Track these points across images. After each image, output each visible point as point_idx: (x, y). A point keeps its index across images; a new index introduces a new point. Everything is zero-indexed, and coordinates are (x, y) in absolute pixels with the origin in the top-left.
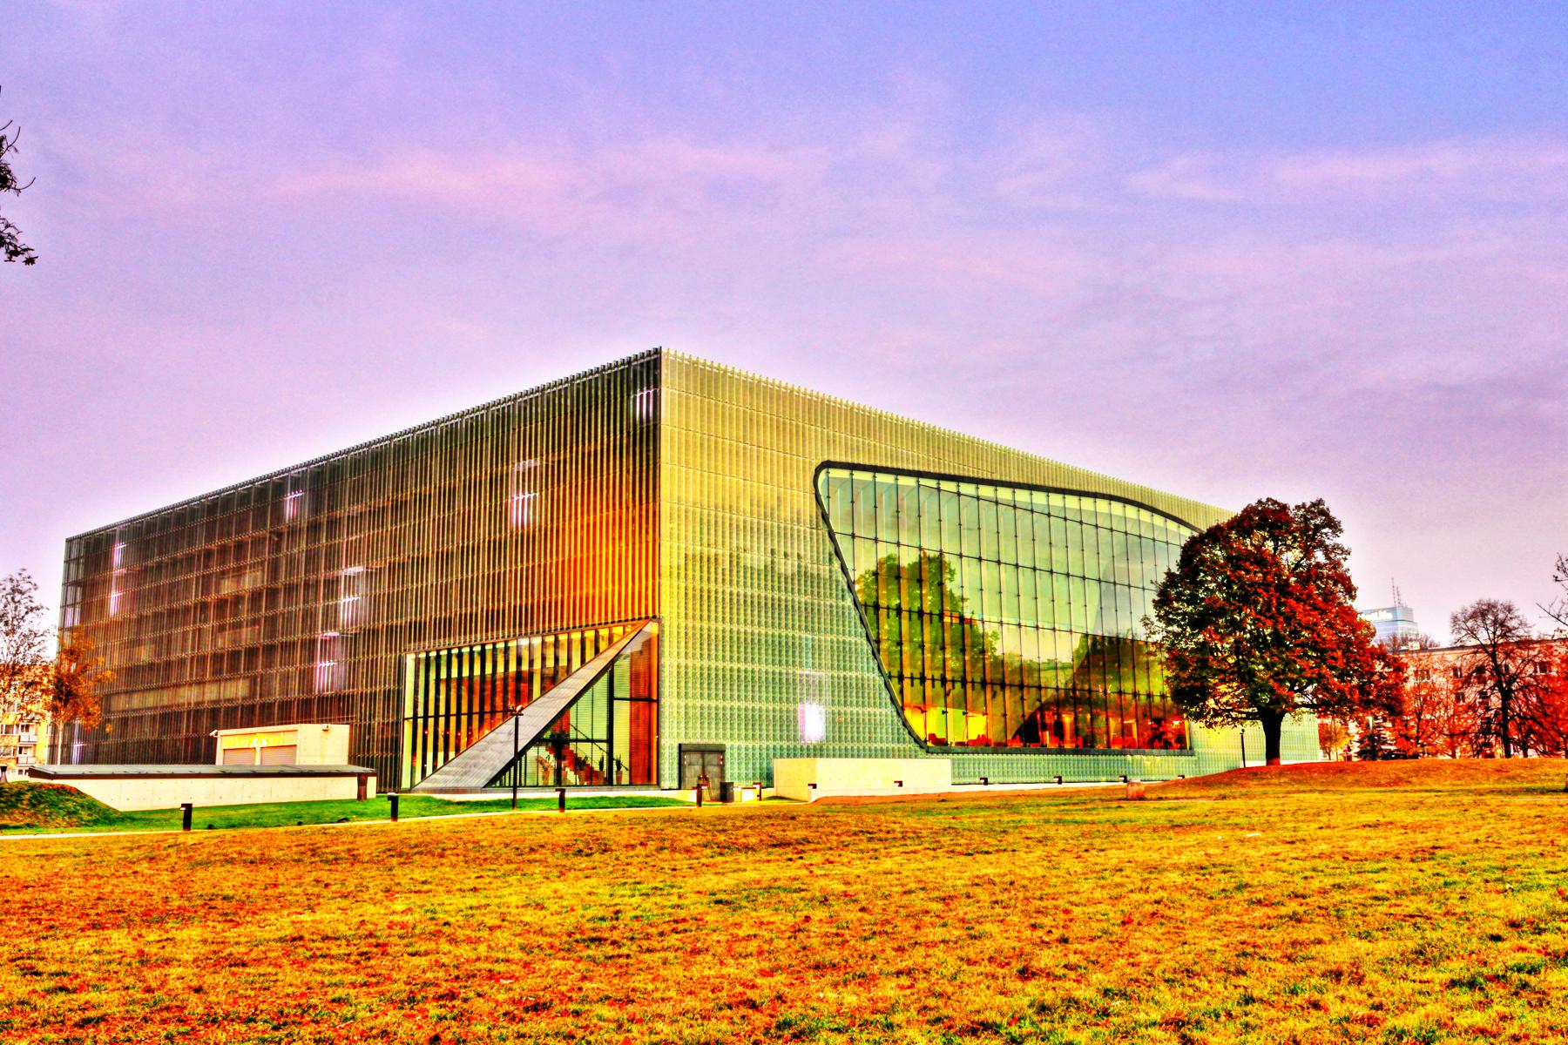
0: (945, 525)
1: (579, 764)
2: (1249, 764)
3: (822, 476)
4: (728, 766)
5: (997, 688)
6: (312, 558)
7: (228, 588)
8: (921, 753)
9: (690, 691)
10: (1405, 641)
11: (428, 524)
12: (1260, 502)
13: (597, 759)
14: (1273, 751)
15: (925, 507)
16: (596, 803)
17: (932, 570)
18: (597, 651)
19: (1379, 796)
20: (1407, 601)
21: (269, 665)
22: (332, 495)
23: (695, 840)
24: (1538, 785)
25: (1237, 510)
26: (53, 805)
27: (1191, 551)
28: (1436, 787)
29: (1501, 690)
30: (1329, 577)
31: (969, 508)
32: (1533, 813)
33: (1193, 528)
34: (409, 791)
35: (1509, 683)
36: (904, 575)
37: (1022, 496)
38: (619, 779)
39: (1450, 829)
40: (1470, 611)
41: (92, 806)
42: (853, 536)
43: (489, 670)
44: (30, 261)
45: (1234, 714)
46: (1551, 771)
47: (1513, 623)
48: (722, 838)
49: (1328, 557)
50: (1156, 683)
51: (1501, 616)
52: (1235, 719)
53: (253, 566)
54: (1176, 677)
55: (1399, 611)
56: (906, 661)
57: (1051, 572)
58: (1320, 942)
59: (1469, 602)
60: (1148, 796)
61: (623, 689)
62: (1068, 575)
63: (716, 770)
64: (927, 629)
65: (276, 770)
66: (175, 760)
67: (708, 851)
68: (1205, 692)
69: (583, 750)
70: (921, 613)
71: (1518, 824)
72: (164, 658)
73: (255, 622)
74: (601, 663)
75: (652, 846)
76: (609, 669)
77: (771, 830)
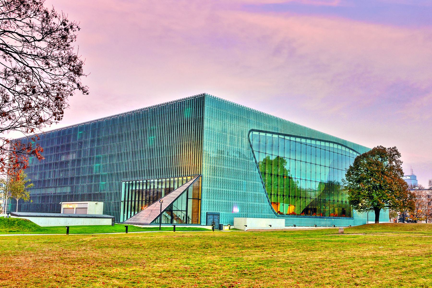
0: (286, 149)
1: (178, 219)
2: (369, 222)
3: (251, 134)
4: (220, 219)
5: (299, 198)
6: (92, 150)
7: (63, 158)
8: (276, 217)
10: (415, 187)
11: (130, 142)
12: (378, 147)
13: (183, 215)
14: (377, 219)
16: (183, 229)
17: (280, 161)
18: (182, 184)
19: (408, 235)
20: (415, 173)
23: (234, 245)
26: (24, 225)
27: (357, 160)
28: (423, 232)
31: (298, 146)
33: (357, 153)
34: (122, 223)
36: (273, 164)
37: (309, 141)
38: (189, 222)
41: (35, 225)
42: (259, 152)
43: (148, 188)
44: (88, 94)
45: (366, 208)
48: (241, 244)
49: (396, 164)
50: (345, 197)
53: (73, 153)
54: (351, 197)
55: (413, 177)
57: (316, 164)
58: (415, 279)
60: (344, 232)
61: (190, 196)
62: (321, 165)
63: (217, 220)
64: (279, 180)
67: (238, 248)
68: (358, 202)
69: (179, 213)
70: (278, 176)
73: (73, 169)
74: (184, 188)
76: (187, 190)
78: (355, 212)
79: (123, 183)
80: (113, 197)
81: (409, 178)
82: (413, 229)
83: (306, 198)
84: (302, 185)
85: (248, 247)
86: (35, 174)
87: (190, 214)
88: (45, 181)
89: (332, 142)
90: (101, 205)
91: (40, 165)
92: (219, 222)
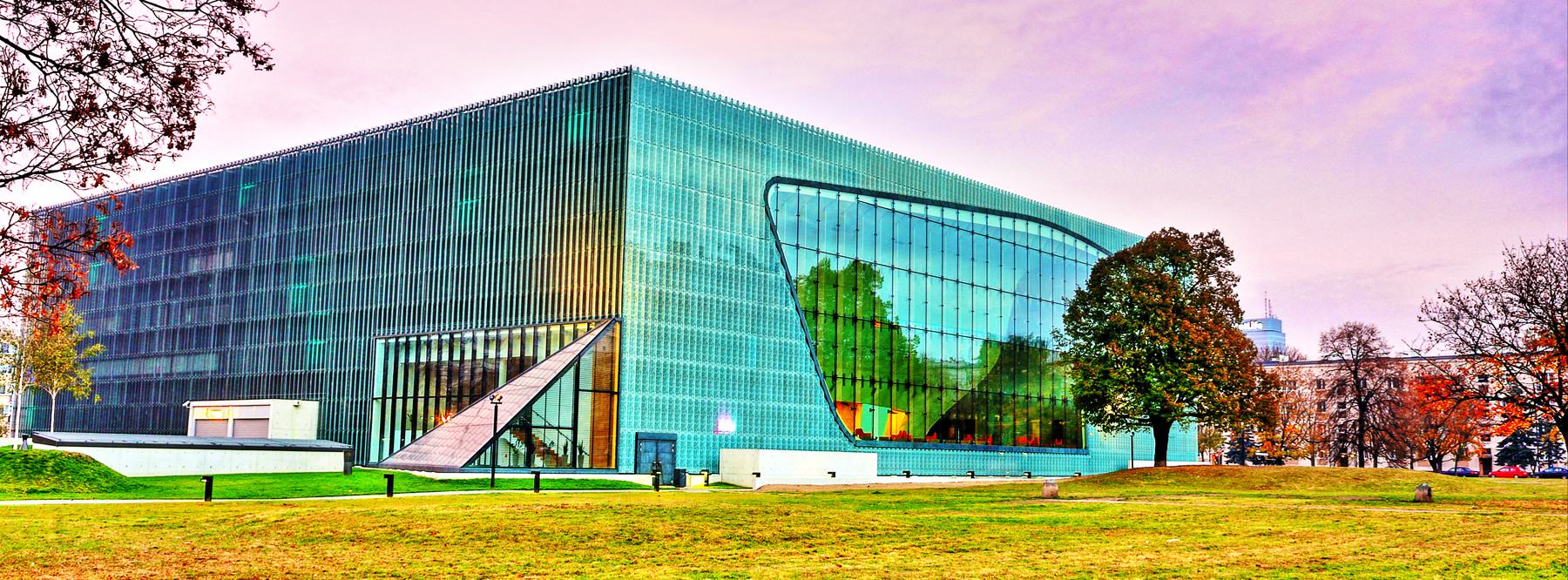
1: (547, 452)
2: (1138, 464)
3: (772, 190)
5: (919, 389)
6: (282, 242)
7: (195, 267)
8: (851, 447)
9: (648, 385)
10: (1277, 353)
11: (400, 217)
13: (563, 441)
14: (1161, 455)
15: (863, 220)
17: (862, 275)
18: (562, 347)
19: (1257, 502)
20: (1278, 313)
21: (239, 341)
22: (303, 186)
23: (719, 533)
24: (1390, 494)
25: (1143, 233)
26: (75, 472)
28: (1301, 492)
29: (1360, 404)
30: (1220, 301)
32: (1393, 525)
34: (377, 465)
35: (1367, 398)
36: (841, 283)
37: (950, 214)
39: (1330, 538)
40: (1338, 332)
41: (107, 474)
42: (798, 247)
43: (457, 357)
44: (269, 68)
46: (1402, 481)
47: (1375, 345)
48: (741, 532)
50: (1062, 387)
51: (1365, 338)
52: (1129, 425)
53: (225, 249)
54: (1081, 385)
56: (839, 362)
59: (1338, 325)
61: (586, 382)
63: (668, 457)
64: (859, 333)
65: (262, 443)
66: (143, 431)
67: (733, 543)
68: (1104, 400)
69: (551, 436)
70: (855, 320)
71: (1384, 537)
72: (132, 329)
73: (226, 301)
74: (567, 357)
75: (687, 538)
76: (576, 363)
77: (779, 525)
78: (1093, 432)
79: (380, 344)
80: (349, 385)
81: (1260, 326)
82: (1272, 484)
83: (941, 389)
84: (930, 349)
85: (764, 541)
86: (108, 315)
87: (584, 438)
88: (137, 336)
89: (1022, 217)
90: (310, 409)
91: (123, 289)
92: (674, 464)
